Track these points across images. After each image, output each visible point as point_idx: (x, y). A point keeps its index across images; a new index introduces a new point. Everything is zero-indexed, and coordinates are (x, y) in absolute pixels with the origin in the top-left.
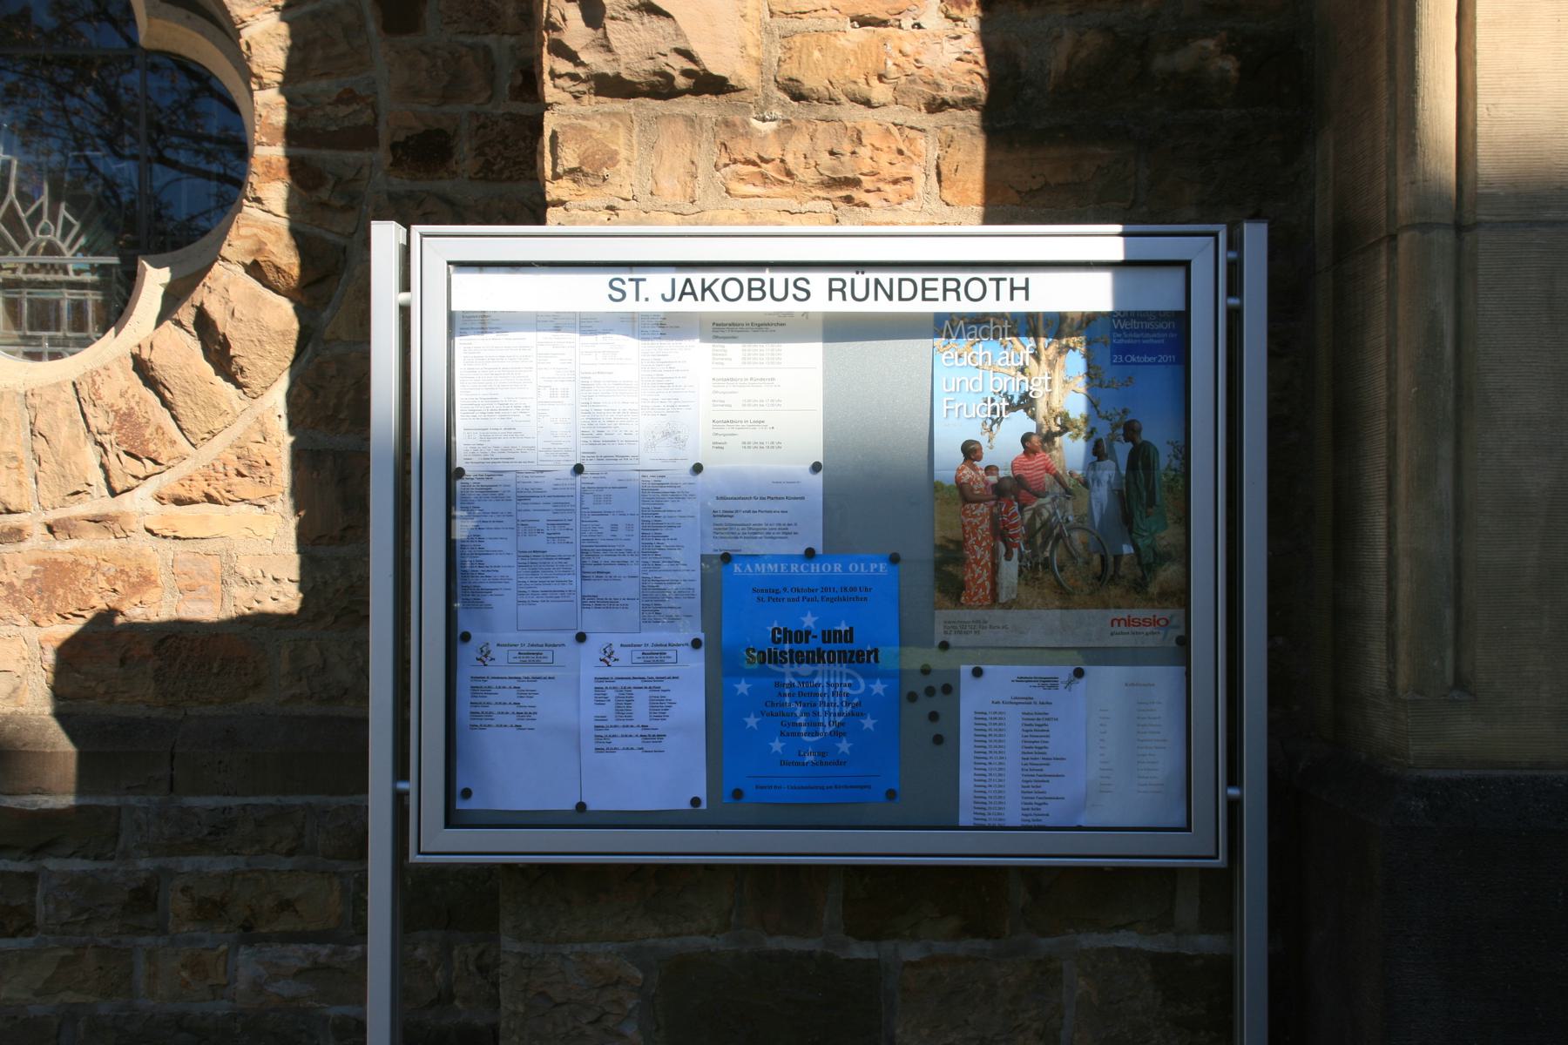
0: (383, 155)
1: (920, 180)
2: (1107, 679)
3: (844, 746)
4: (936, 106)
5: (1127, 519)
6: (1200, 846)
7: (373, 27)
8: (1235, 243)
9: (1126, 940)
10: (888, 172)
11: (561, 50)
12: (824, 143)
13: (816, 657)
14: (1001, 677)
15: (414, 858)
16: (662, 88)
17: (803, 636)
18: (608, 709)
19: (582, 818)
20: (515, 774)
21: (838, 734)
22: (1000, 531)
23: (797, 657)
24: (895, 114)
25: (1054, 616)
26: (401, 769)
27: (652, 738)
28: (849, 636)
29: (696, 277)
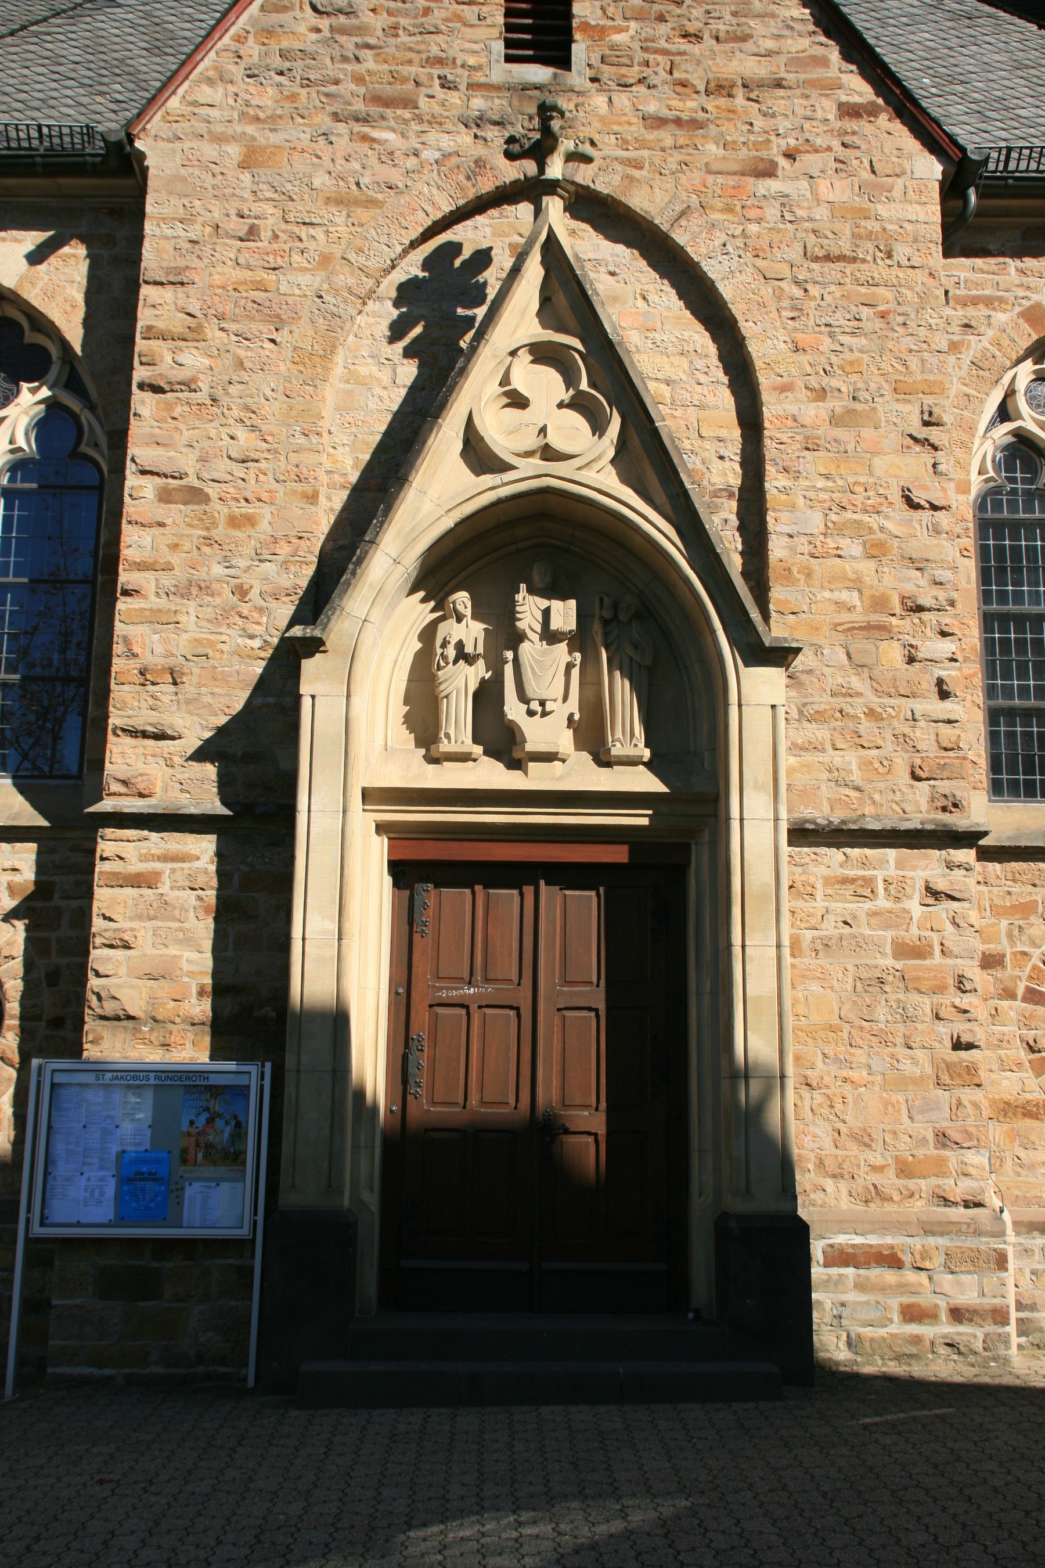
0: (43, 1024)
1: (188, 1045)
2: (225, 1186)
3: (152, 1205)
4: (193, 1024)
5: (233, 1141)
6: (245, 1232)
7: (44, 985)
8: (263, 1066)
9: (230, 1261)
10: (179, 1042)
11: (90, 1007)
12: (162, 1034)
13: (146, 1180)
14: (197, 1186)
15: (31, 1235)
16: (118, 1018)
17: (143, 1173)
18: (87, 1194)
19: (78, 1224)
20: (62, 1211)
21: (151, 1201)
22: (198, 1145)
23: (141, 1180)
24: (182, 1026)
25: (212, 1168)
26: (29, 1211)
27: (99, 1202)
28: (155, 1174)
29: (119, 1074)
